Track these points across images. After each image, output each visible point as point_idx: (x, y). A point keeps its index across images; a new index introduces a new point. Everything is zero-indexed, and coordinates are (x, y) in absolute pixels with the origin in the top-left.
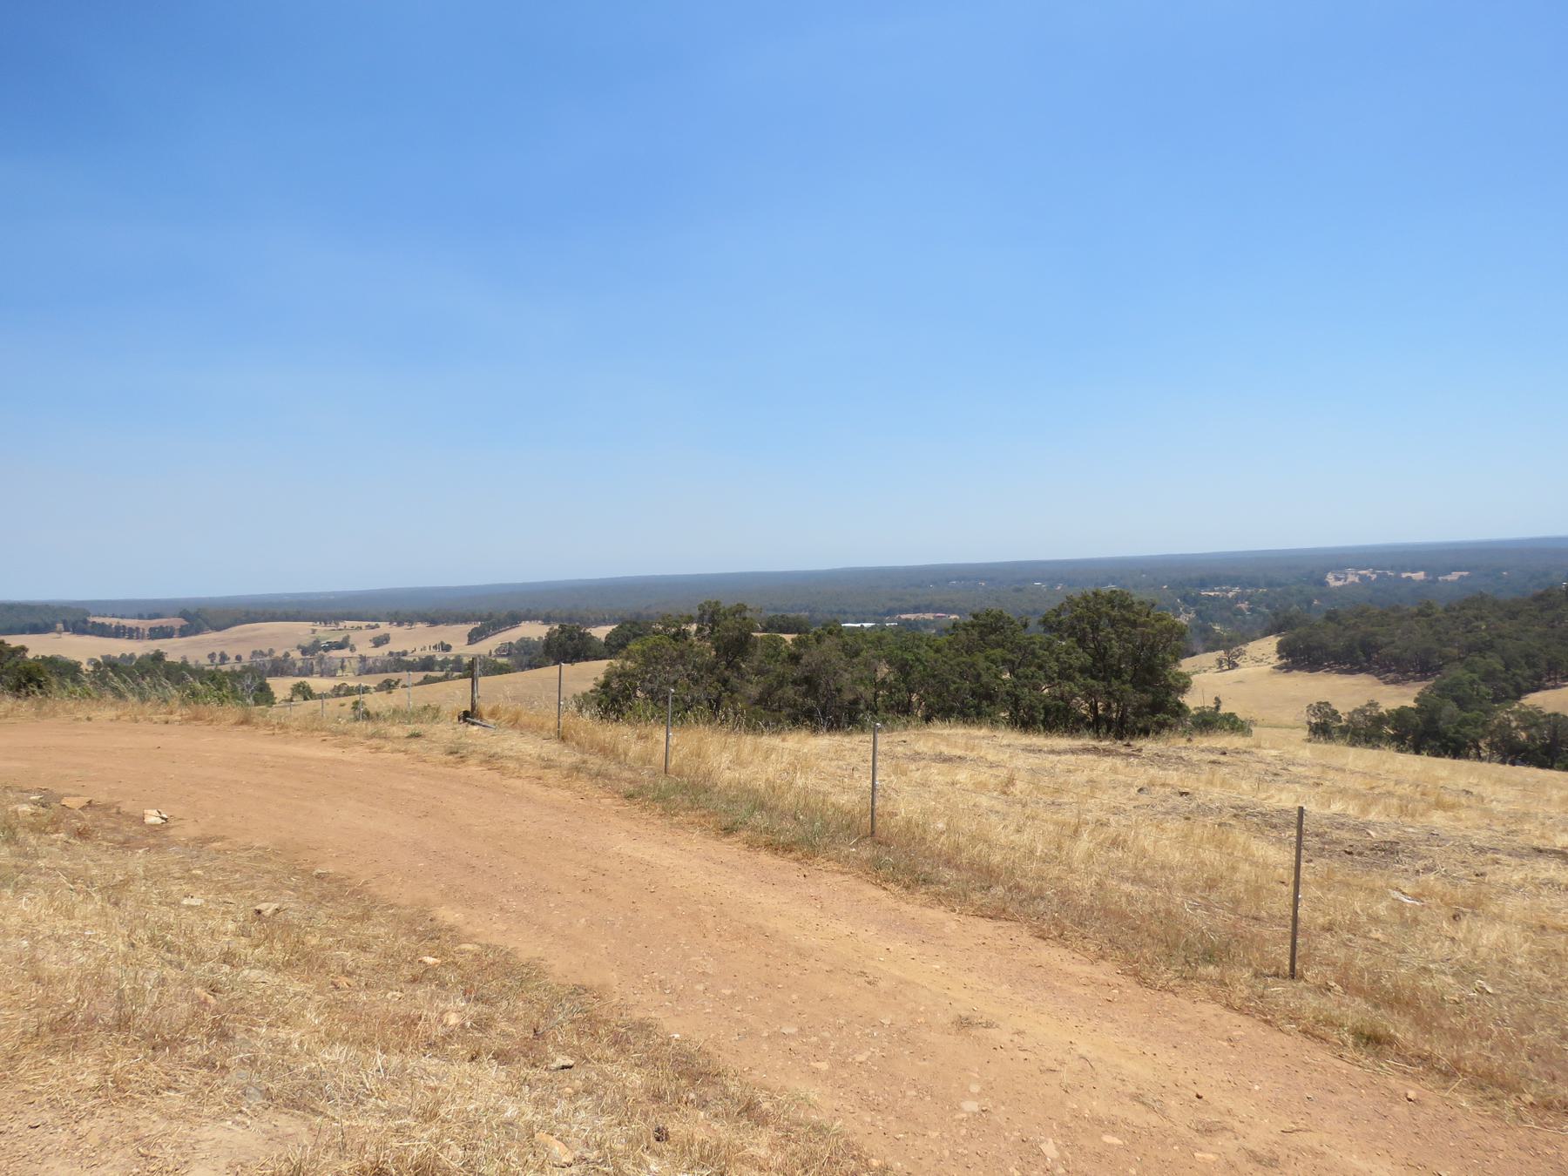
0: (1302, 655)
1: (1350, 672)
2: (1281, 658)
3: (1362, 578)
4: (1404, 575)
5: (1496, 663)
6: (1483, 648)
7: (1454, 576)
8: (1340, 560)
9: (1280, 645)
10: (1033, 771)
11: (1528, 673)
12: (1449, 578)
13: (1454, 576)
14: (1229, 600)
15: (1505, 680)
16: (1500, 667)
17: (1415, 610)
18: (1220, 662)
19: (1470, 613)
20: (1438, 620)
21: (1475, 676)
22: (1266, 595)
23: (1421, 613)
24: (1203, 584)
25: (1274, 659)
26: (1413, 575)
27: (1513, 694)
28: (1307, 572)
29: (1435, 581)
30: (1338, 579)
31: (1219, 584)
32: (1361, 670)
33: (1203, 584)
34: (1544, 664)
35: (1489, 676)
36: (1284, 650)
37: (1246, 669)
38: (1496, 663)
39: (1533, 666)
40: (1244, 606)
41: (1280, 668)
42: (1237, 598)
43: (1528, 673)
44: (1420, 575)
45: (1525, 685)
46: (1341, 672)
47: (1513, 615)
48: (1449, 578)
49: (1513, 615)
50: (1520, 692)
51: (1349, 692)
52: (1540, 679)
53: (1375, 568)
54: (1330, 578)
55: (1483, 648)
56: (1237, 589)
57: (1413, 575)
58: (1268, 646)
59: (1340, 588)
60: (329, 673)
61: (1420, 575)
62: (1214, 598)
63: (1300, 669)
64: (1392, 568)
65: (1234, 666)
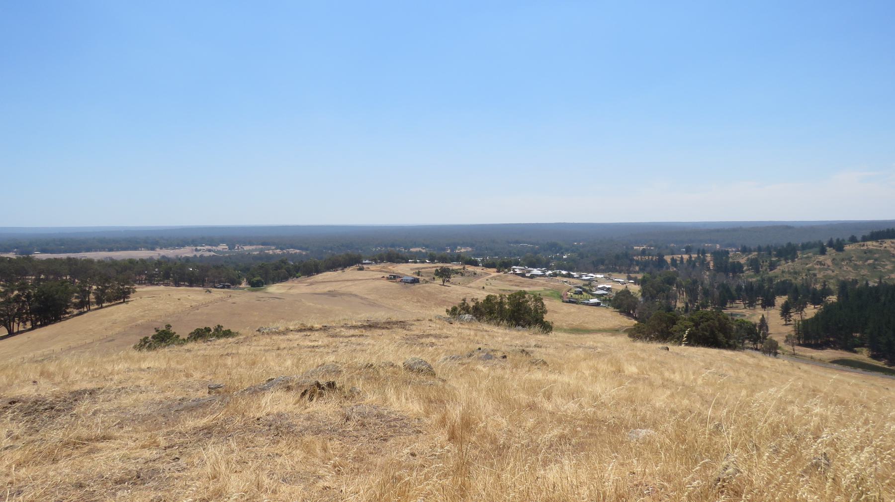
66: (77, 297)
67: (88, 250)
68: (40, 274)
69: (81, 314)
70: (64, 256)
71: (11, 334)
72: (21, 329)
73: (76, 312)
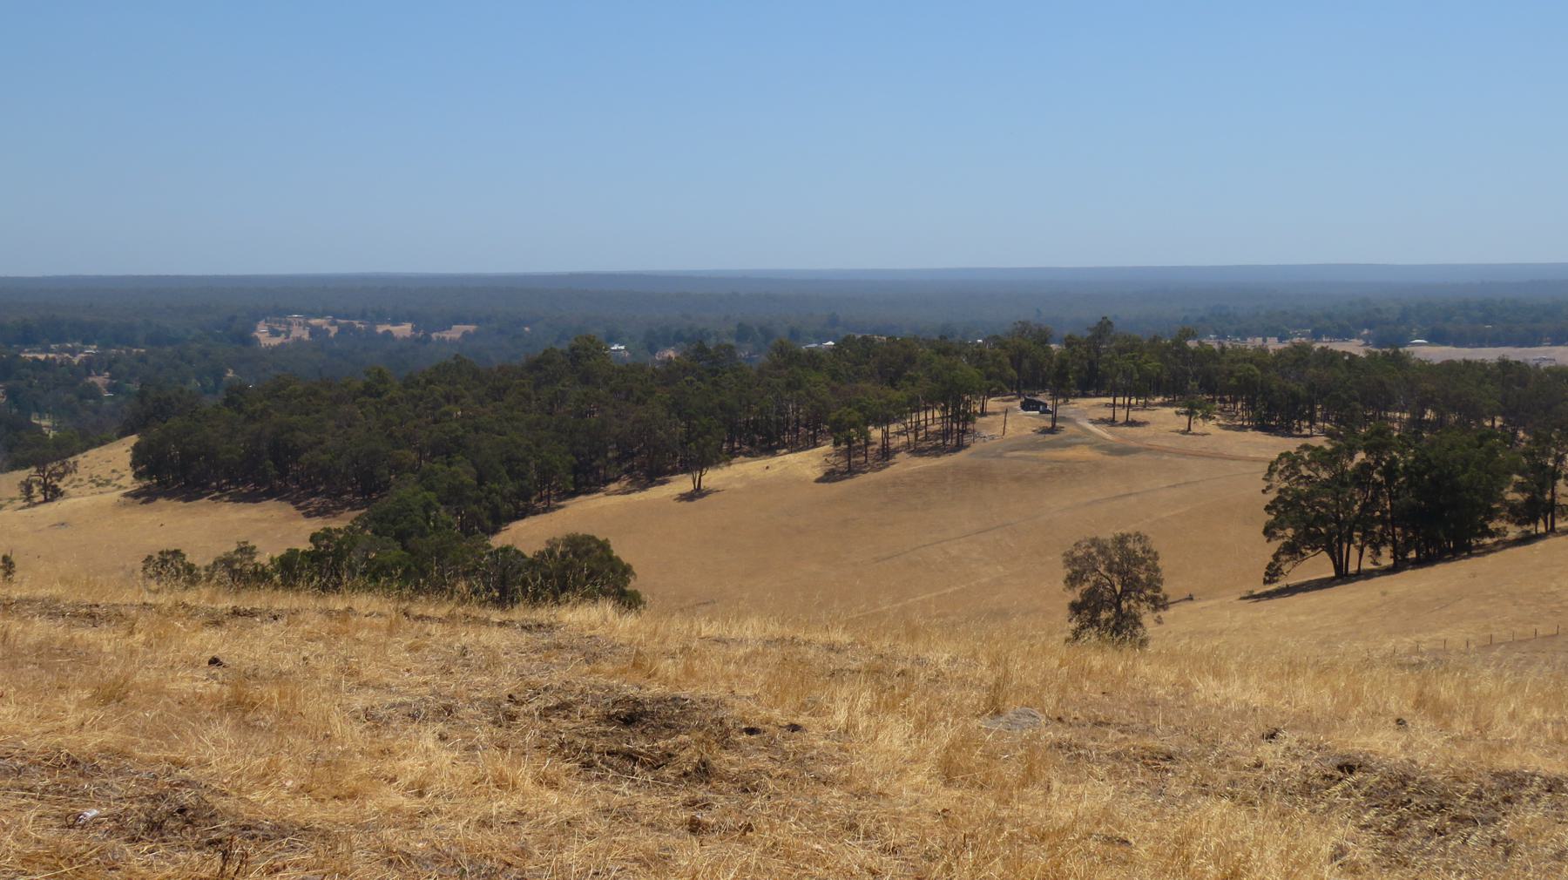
0: (170, 474)
1: (253, 498)
2: (138, 476)
3: (315, 331)
4: (381, 329)
5: (463, 472)
6: (446, 449)
7: (456, 332)
8: (280, 298)
9: (136, 449)
10: (1149, 730)
11: (511, 487)
12: (448, 335)
13: (456, 332)
14: (73, 370)
15: (478, 501)
16: (469, 479)
17: (359, 385)
18: (27, 487)
19: (439, 390)
20: (392, 402)
21: (431, 496)
22: (142, 359)
23: (368, 390)
24: (28, 337)
25: (129, 482)
26: (395, 329)
27: (489, 524)
28: (216, 321)
29: (427, 340)
30: (274, 333)
31: (60, 338)
32: (269, 495)
33: (28, 337)
34: (533, 475)
35: (453, 497)
36: (145, 462)
37: (78, 501)
38: (463, 472)
39: (515, 475)
40: (100, 380)
41: (135, 495)
42: (89, 366)
43: (511, 487)
44: (404, 330)
45: (506, 507)
46: (238, 498)
47: (498, 393)
48: (448, 335)
49: (498, 393)
50: (499, 521)
51: (207, 527)
52: (527, 498)
53: (336, 316)
54: (262, 334)
55: (446, 449)
56: (92, 350)
57: (395, 329)
58: (117, 456)
59: (274, 350)
60: (1492, 535)
61: (404, 330)
62: (46, 365)
63: (170, 495)
64: (363, 316)
65: (53, 494)
66: (1520, 488)
67: (1531, 339)
68: (1423, 405)
69: (1527, 539)
70: (1489, 355)
71: (1342, 576)
72: (1367, 565)
73: (1513, 532)
